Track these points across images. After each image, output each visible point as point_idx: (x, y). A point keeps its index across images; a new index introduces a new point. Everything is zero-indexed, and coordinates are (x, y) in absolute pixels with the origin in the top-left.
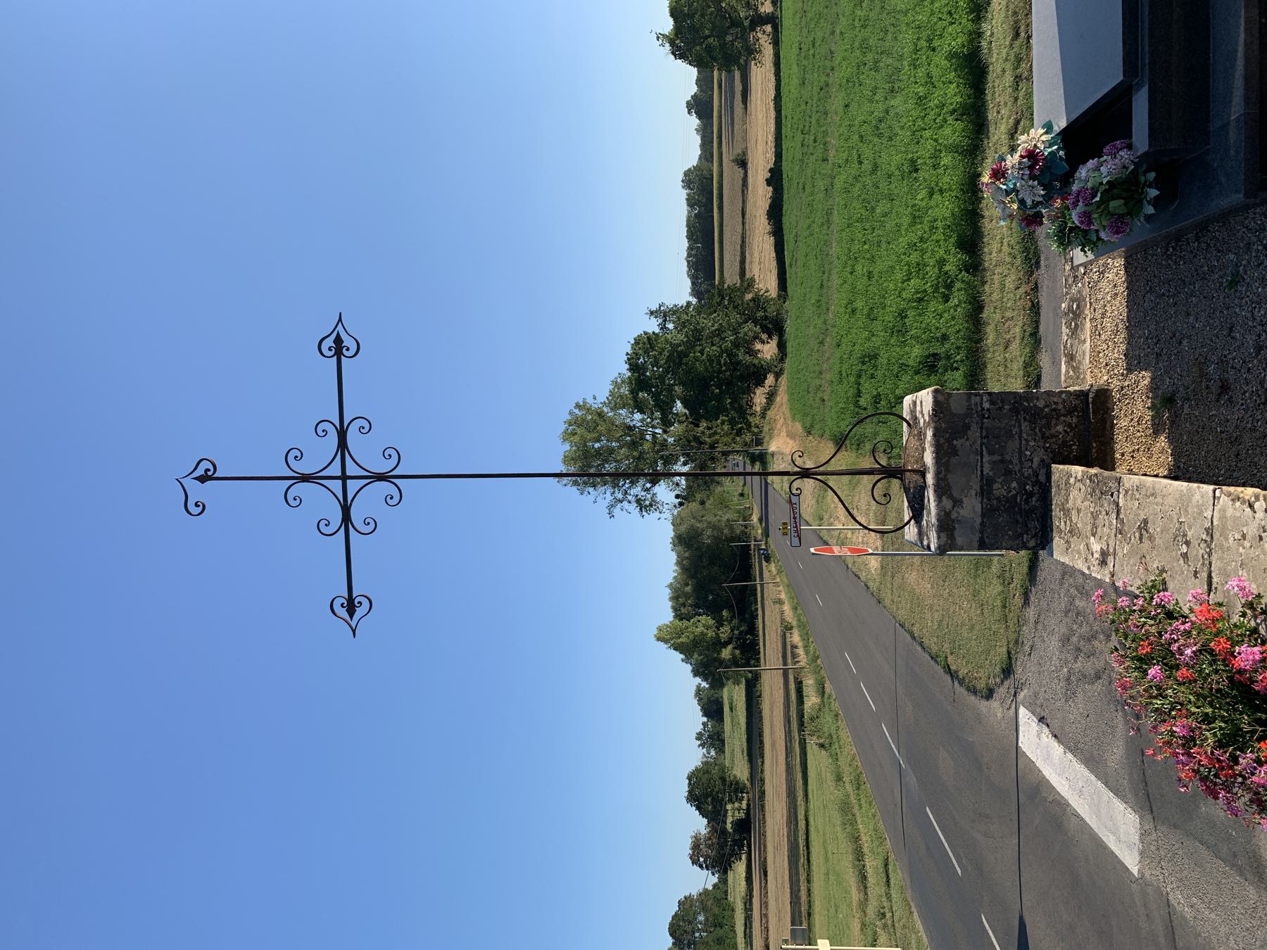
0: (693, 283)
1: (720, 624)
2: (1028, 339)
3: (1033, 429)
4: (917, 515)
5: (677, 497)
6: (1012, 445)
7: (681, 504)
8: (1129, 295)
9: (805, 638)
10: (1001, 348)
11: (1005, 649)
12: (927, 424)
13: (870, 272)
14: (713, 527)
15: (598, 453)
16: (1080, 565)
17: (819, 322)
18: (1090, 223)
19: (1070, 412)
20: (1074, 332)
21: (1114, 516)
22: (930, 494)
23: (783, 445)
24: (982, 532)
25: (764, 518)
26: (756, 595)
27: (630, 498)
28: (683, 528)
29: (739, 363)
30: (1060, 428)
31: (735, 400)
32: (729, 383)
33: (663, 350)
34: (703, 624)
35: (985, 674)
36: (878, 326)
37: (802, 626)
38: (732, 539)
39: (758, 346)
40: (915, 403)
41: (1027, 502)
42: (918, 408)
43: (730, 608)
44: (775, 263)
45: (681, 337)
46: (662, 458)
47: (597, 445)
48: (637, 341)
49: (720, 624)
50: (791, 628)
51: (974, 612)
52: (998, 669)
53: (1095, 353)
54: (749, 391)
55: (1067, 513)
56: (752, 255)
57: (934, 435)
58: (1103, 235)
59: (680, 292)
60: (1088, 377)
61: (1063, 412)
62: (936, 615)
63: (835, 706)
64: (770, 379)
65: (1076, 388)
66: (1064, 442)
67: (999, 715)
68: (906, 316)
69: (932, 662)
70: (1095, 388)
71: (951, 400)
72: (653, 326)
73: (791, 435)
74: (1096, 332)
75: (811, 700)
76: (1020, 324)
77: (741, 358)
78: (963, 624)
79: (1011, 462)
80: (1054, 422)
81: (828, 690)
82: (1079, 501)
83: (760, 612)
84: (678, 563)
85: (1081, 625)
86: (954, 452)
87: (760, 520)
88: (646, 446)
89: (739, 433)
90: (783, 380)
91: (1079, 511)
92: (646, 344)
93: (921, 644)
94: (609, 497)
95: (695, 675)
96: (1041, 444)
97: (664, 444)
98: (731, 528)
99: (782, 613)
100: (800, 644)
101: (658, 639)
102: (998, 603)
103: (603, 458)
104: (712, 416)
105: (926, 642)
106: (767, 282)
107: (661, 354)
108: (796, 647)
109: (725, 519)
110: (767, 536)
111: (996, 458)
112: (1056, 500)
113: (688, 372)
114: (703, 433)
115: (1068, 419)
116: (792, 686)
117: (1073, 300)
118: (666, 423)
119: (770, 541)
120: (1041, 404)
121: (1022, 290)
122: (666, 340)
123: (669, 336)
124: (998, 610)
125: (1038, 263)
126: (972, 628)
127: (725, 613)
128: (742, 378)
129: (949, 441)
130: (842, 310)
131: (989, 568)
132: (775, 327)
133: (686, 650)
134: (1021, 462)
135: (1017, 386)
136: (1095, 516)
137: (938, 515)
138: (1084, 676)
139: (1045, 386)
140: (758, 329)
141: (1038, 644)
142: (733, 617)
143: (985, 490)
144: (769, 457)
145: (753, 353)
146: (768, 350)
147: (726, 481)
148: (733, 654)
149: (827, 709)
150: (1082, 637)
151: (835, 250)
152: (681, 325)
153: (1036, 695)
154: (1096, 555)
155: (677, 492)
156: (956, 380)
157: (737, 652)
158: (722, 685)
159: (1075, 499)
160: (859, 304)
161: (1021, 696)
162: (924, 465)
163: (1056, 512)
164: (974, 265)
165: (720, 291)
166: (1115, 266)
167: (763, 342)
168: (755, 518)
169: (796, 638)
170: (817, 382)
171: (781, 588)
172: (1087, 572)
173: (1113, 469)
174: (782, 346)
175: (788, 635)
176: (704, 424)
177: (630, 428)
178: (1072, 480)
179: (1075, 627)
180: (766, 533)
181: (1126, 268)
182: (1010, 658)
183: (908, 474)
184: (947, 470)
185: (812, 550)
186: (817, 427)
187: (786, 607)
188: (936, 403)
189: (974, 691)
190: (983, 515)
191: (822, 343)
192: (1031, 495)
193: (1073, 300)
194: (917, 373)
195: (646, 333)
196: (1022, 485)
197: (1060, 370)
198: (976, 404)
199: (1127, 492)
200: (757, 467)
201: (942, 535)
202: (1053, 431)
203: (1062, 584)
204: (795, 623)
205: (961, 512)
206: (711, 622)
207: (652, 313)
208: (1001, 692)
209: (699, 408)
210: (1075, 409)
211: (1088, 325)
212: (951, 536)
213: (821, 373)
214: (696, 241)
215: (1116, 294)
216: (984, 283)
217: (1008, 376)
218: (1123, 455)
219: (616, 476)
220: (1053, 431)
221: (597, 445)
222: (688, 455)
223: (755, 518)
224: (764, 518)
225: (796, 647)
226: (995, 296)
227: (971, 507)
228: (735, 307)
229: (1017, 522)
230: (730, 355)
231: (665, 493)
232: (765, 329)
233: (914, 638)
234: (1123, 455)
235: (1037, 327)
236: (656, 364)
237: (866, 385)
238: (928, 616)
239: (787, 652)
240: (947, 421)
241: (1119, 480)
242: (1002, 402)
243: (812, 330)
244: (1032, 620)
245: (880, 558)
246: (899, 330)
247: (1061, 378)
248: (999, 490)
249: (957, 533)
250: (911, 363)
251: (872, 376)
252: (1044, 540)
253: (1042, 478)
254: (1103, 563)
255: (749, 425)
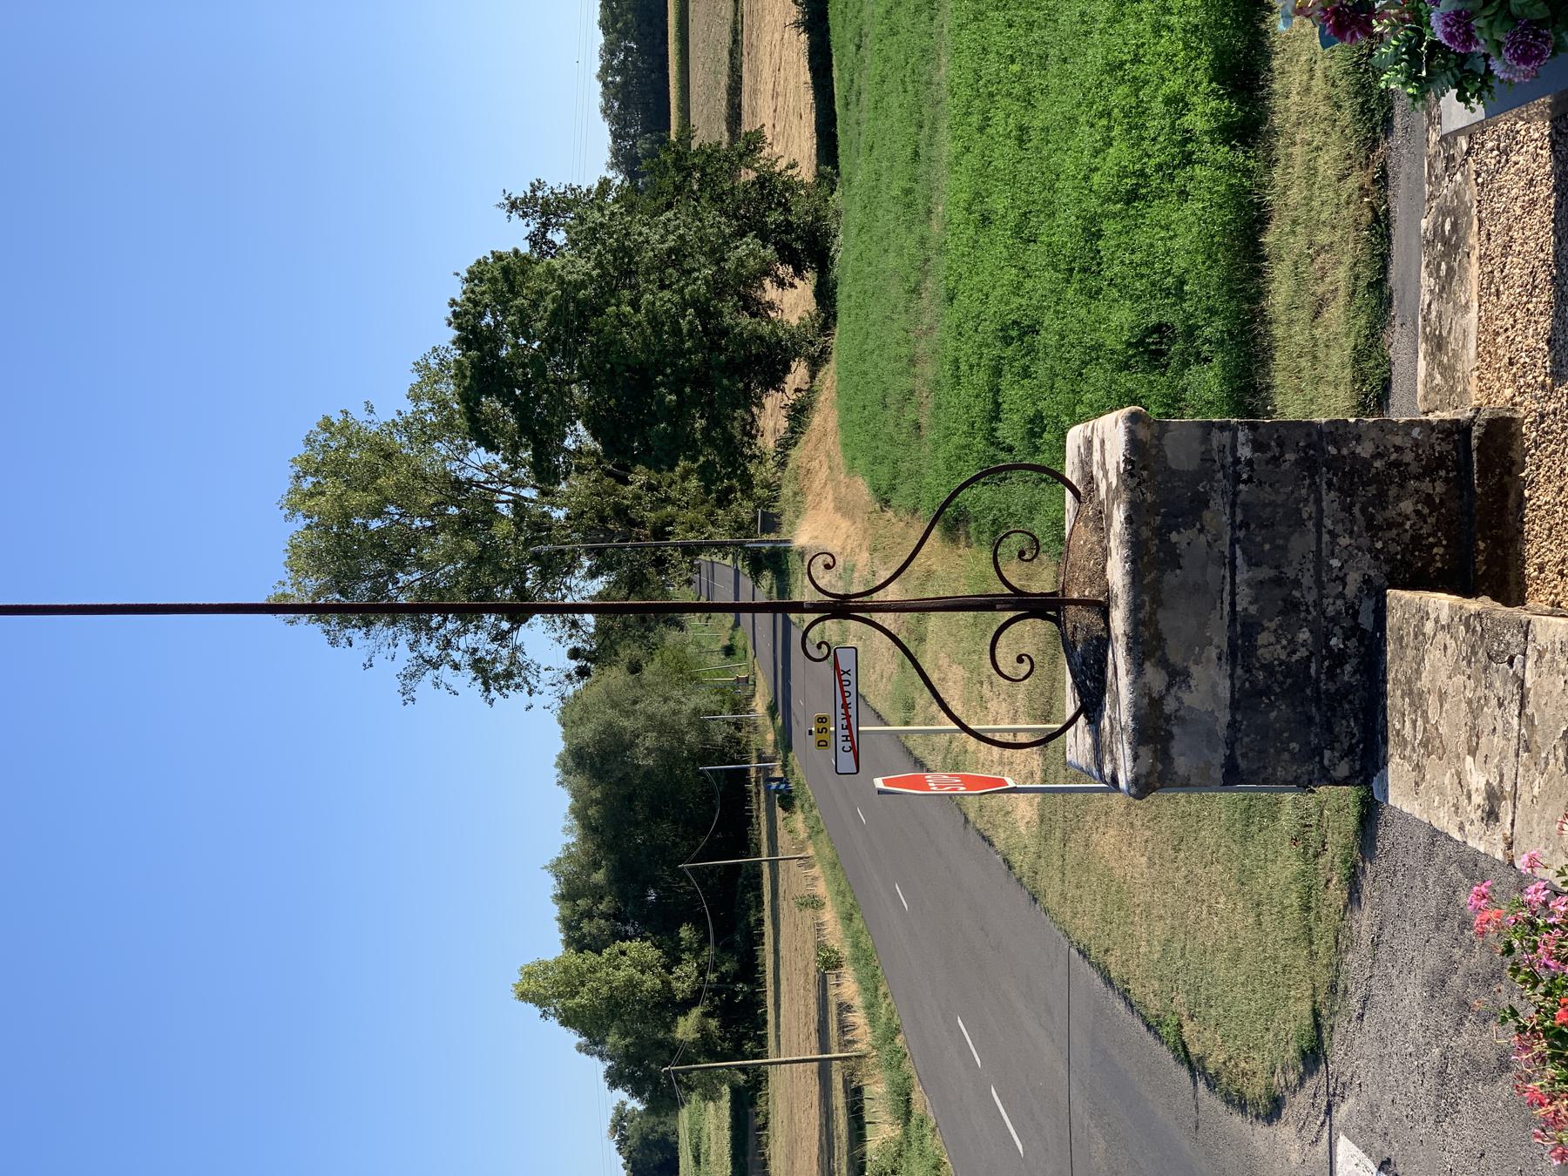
0: (616, 136)
1: (673, 959)
2: (1364, 298)
3: (1348, 509)
4: (1091, 706)
5: (574, 654)
6: (1301, 544)
7: (583, 672)
8: (1558, 205)
9: (870, 987)
10: (1304, 315)
11: (1305, 1007)
12: (1114, 494)
13: (1021, 128)
14: (661, 726)
15: (379, 543)
16: (1445, 821)
17: (910, 242)
18: (1469, 38)
19: (1429, 471)
20: (1446, 285)
21: (1514, 709)
22: (1119, 658)
23: (829, 529)
24: (1231, 743)
25: (781, 706)
26: (758, 887)
27: (456, 656)
28: (587, 732)
29: (725, 332)
30: (1407, 506)
31: (715, 421)
32: (702, 380)
33: (541, 294)
34: (633, 961)
35: (1265, 1063)
36: (1036, 256)
37: (862, 957)
38: (705, 756)
39: (771, 292)
40: (1089, 442)
41: (1331, 675)
42: (1096, 456)
43: (699, 922)
44: (809, 97)
45: (585, 266)
46: (536, 557)
47: (375, 524)
48: (475, 276)
49: (673, 959)
50: (838, 965)
51: (1243, 920)
52: (1292, 1052)
53: (1489, 335)
54: (748, 400)
55: (1417, 700)
56: (756, 75)
57: (1129, 520)
58: (1497, 67)
59: (583, 153)
60: (1473, 389)
61: (1414, 468)
62: (1159, 929)
63: (934, 1144)
64: (798, 374)
65: (1447, 415)
66: (1417, 539)
67: (1295, 1157)
68: (1099, 235)
69: (1150, 1038)
70: (1485, 415)
71: (1168, 440)
72: (514, 236)
73: (844, 508)
74: (1490, 288)
75: (882, 1133)
76: (1347, 260)
77: (727, 320)
78: (1217, 949)
79: (1297, 583)
80: (1393, 491)
81: (917, 1109)
82: (1443, 675)
83: (768, 928)
84: (579, 813)
85: (1469, 951)
86: (1171, 559)
87: (772, 710)
88: (501, 529)
89: (724, 500)
90: (829, 374)
91: (1442, 696)
92: (499, 280)
93: (1125, 995)
94: (404, 653)
95: (613, 1084)
96: (1364, 541)
97: (542, 526)
98: (703, 729)
99: (819, 927)
100: (858, 1002)
101: (524, 996)
102: (1293, 899)
103: (390, 561)
104: (661, 459)
105: (1136, 990)
106: (791, 145)
107: (535, 305)
108: (849, 1008)
109: (688, 708)
110: (788, 747)
111: (1265, 573)
112: (1395, 671)
113: (600, 352)
114: (638, 497)
115: (1426, 486)
116: (839, 1100)
117: (1444, 212)
118: (546, 475)
119: (795, 759)
120: (1365, 450)
121: (1352, 183)
122: (551, 271)
123: (556, 263)
124: (1294, 913)
125: (1388, 121)
126: (1236, 957)
127: (685, 932)
128: (737, 368)
129: (1161, 533)
130: (959, 216)
131: (1274, 818)
132: (809, 250)
133: (591, 1024)
134: (1320, 584)
135: (1330, 402)
136: (1475, 709)
137: (1135, 704)
138: (1476, 1065)
139: (1399, 413)
140: (769, 252)
141: (1379, 993)
142: (703, 942)
143: (1240, 651)
144: (794, 563)
145: (759, 309)
146: (793, 302)
147: (693, 620)
148: (702, 1029)
149: (915, 1152)
150: (1472, 976)
151: (945, 71)
152: (586, 238)
153: (1373, 1109)
154: (1478, 799)
155: (572, 644)
156: (1206, 382)
157: (713, 1023)
158: (675, 1105)
159: (1435, 669)
160: (998, 203)
161: (1342, 1112)
162: (1107, 589)
163: (1395, 699)
164: (1248, 126)
165: (680, 157)
166: (1532, 133)
167: (781, 284)
168: (760, 705)
169: (848, 987)
170: (905, 383)
171: (816, 871)
172: (1457, 836)
173: (1521, 601)
174: (825, 294)
175: (831, 980)
176: (640, 476)
177: (457, 485)
178: (1429, 627)
179: (1458, 953)
180: (785, 741)
181: (1553, 144)
182: (1318, 1026)
183: (1071, 610)
184: (1157, 602)
185: (879, 783)
186: (905, 489)
187: (829, 916)
188: (1134, 444)
189: (1240, 1103)
190: (1235, 705)
191: (915, 291)
192: (1339, 658)
193: (1444, 212)
194: (1125, 366)
195: (498, 257)
196: (1321, 637)
197: (1415, 374)
198: (1222, 450)
199: (1541, 655)
200: (764, 590)
201: (1143, 751)
202: (1391, 513)
203: (1429, 856)
204: (846, 952)
205: (1188, 698)
206: (652, 954)
207: (514, 205)
208: (1298, 1104)
209: (623, 441)
210: (1441, 462)
211: (1474, 270)
212: (1164, 756)
213: (912, 362)
214: (624, 34)
215: (1533, 202)
216: (1271, 163)
217: (1318, 380)
218: (1541, 569)
219: (418, 612)
220: (1391, 513)
221: (375, 524)
222: (599, 552)
223: (760, 705)
224: (781, 706)
225: (849, 1008)
226: (1295, 196)
227: (1208, 688)
228: (717, 199)
229: (1310, 719)
230: (704, 312)
231: (543, 644)
232: (787, 255)
233: (1109, 981)
234: (1541, 569)
235: (1384, 269)
236: (523, 328)
237: (1012, 394)
238: (1141, 931)
239: (828, 1020)
240: (1161, 491)
241: (1525, 629)
242: (1281, 444)
243: (892, 261)
244: (1366, 938)
245: (1038, 798)
246: (1084, 267)
247: (1422, 396)
248: (1270, 648)
249: (1176, 748)
250: (1110, 342)
251: (1026, 373)
252: (1366, 760)
253: (1366, 621)
254: (1491, 815)
255: (747, 483)
